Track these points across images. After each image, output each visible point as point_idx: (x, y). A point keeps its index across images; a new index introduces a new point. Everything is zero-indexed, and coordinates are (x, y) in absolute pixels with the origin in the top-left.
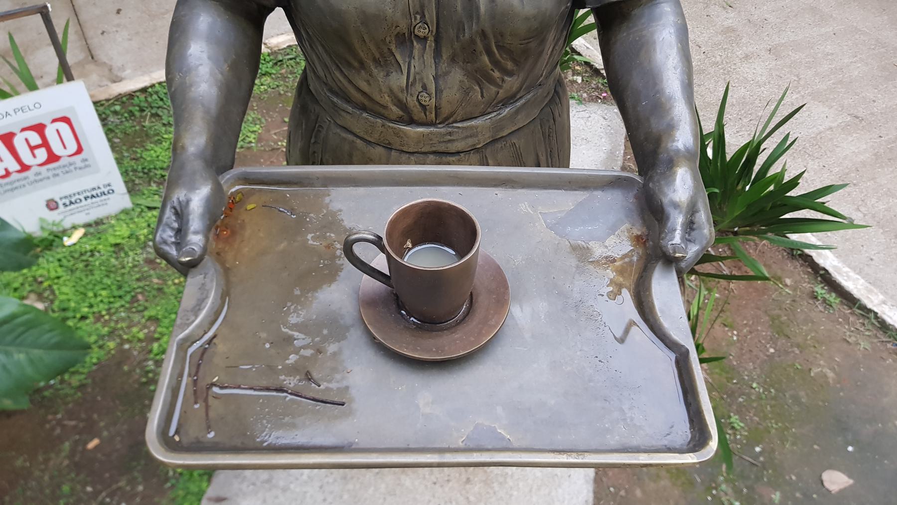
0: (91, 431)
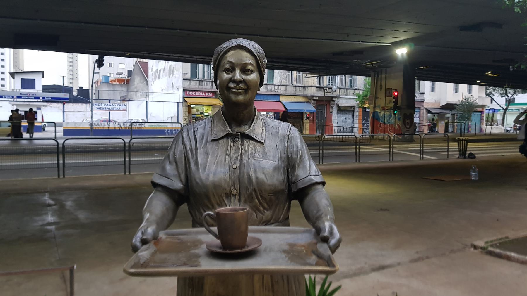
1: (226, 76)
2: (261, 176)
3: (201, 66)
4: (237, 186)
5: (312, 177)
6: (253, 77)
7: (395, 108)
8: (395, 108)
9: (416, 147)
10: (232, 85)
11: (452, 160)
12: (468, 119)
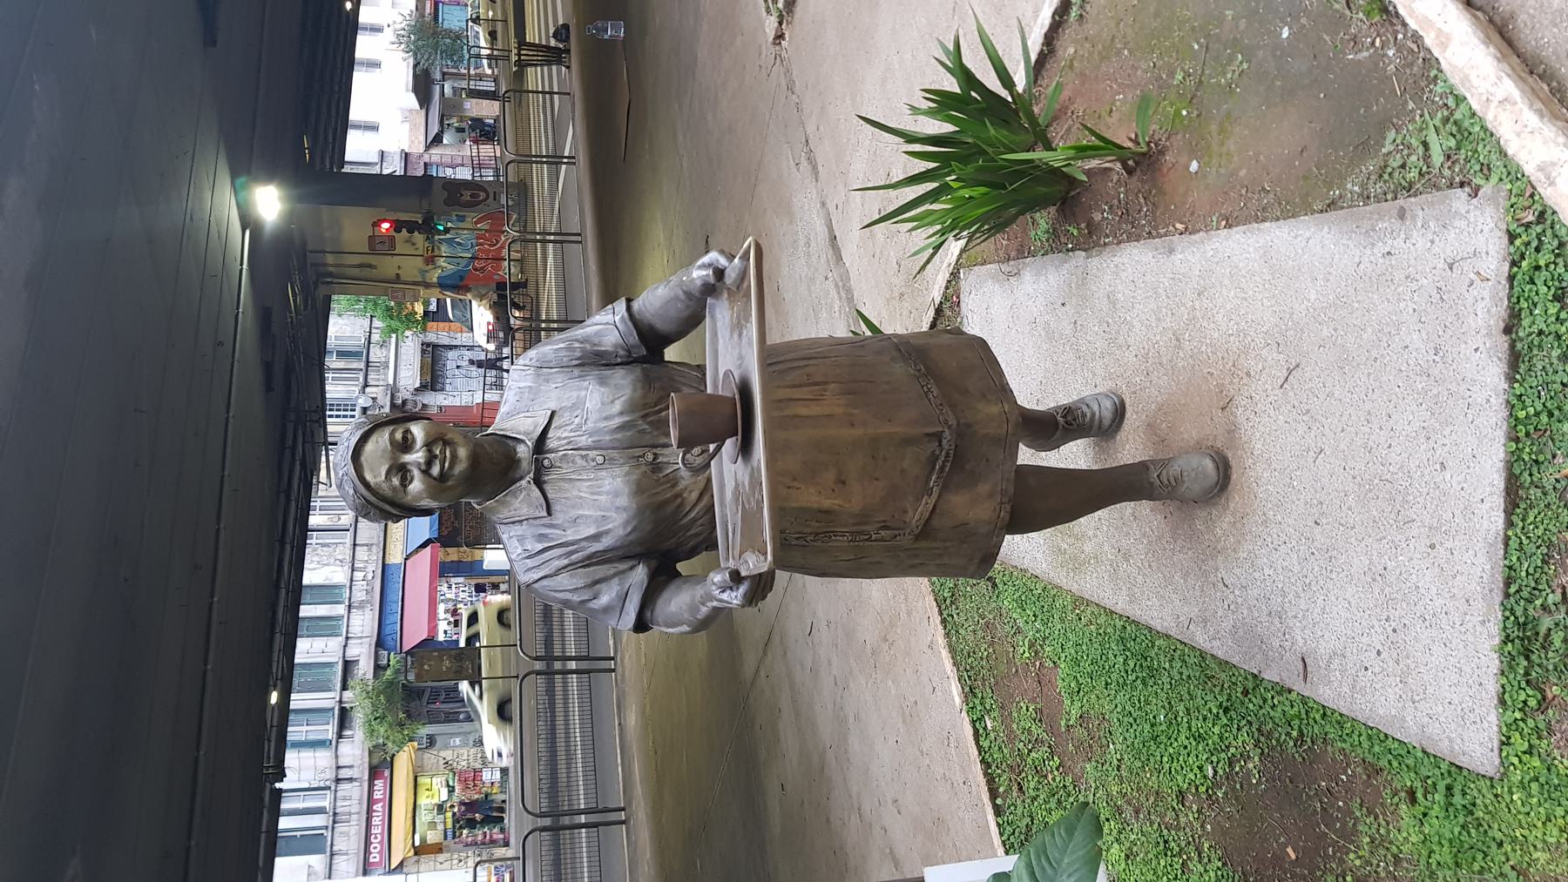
0: (1280, 858)
1: (417, 485)
2: (617, 407)
3: (284, 823)
5: (617, 318)
6: (418, 431)
7: (427, 227)
8: (427, 227)
9: (540, 176)
10: (436, 470)
11: (576, 87)
12: (458, 37)
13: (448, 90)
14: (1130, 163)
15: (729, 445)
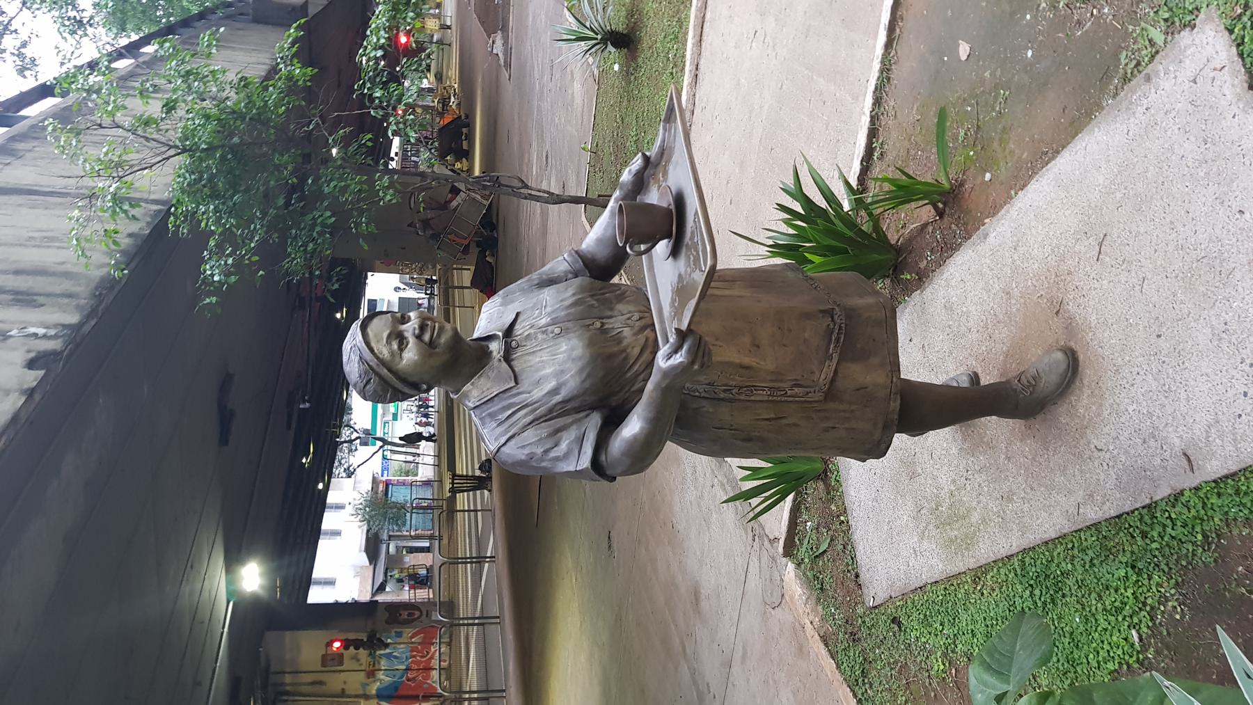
2: (570, 292)
4: (588, 322)
10: (427, 337)
13: (392, 549)
14: (940, 205)
15: (662, 247)
